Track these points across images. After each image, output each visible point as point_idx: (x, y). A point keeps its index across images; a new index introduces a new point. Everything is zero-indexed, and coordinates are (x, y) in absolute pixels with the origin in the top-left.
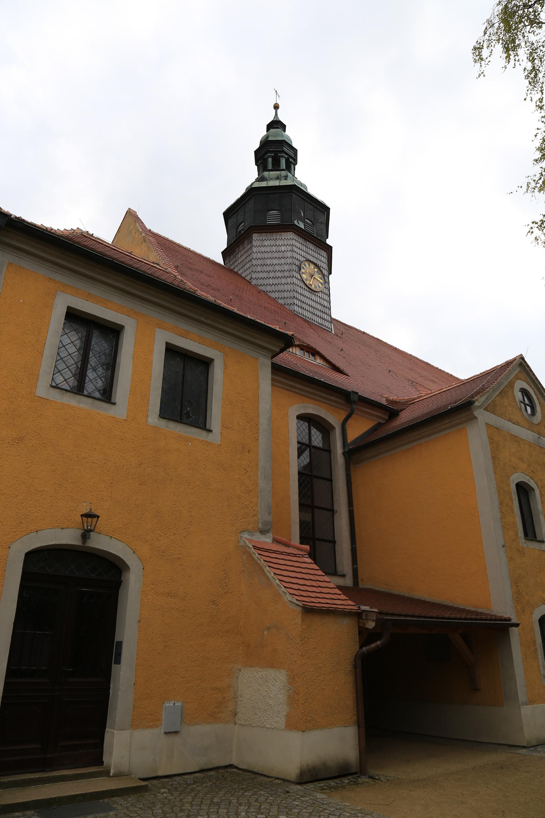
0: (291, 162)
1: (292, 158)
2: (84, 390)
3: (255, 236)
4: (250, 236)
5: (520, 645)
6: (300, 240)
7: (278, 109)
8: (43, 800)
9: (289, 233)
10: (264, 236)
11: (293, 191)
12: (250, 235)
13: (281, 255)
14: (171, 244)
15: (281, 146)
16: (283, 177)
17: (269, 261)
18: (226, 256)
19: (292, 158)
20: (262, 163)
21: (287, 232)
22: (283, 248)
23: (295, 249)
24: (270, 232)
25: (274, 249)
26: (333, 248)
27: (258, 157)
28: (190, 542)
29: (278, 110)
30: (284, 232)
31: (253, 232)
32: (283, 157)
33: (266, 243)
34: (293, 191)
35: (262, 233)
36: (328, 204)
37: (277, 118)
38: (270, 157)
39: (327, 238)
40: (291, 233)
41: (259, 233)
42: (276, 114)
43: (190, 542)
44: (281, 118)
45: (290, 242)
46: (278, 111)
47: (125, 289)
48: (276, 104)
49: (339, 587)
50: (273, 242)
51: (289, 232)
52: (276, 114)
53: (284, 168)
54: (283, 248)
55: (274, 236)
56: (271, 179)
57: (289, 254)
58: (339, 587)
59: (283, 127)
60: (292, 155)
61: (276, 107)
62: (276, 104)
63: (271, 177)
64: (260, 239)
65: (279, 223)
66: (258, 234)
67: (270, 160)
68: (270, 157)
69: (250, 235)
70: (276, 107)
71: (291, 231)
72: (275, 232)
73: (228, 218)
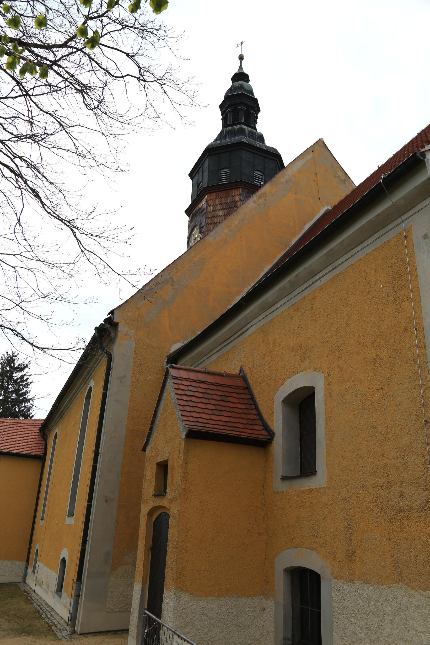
29: (243, 61)
42: (241, 67)
46: (243, 61)
61: (241, 58)
70: (241, 58)
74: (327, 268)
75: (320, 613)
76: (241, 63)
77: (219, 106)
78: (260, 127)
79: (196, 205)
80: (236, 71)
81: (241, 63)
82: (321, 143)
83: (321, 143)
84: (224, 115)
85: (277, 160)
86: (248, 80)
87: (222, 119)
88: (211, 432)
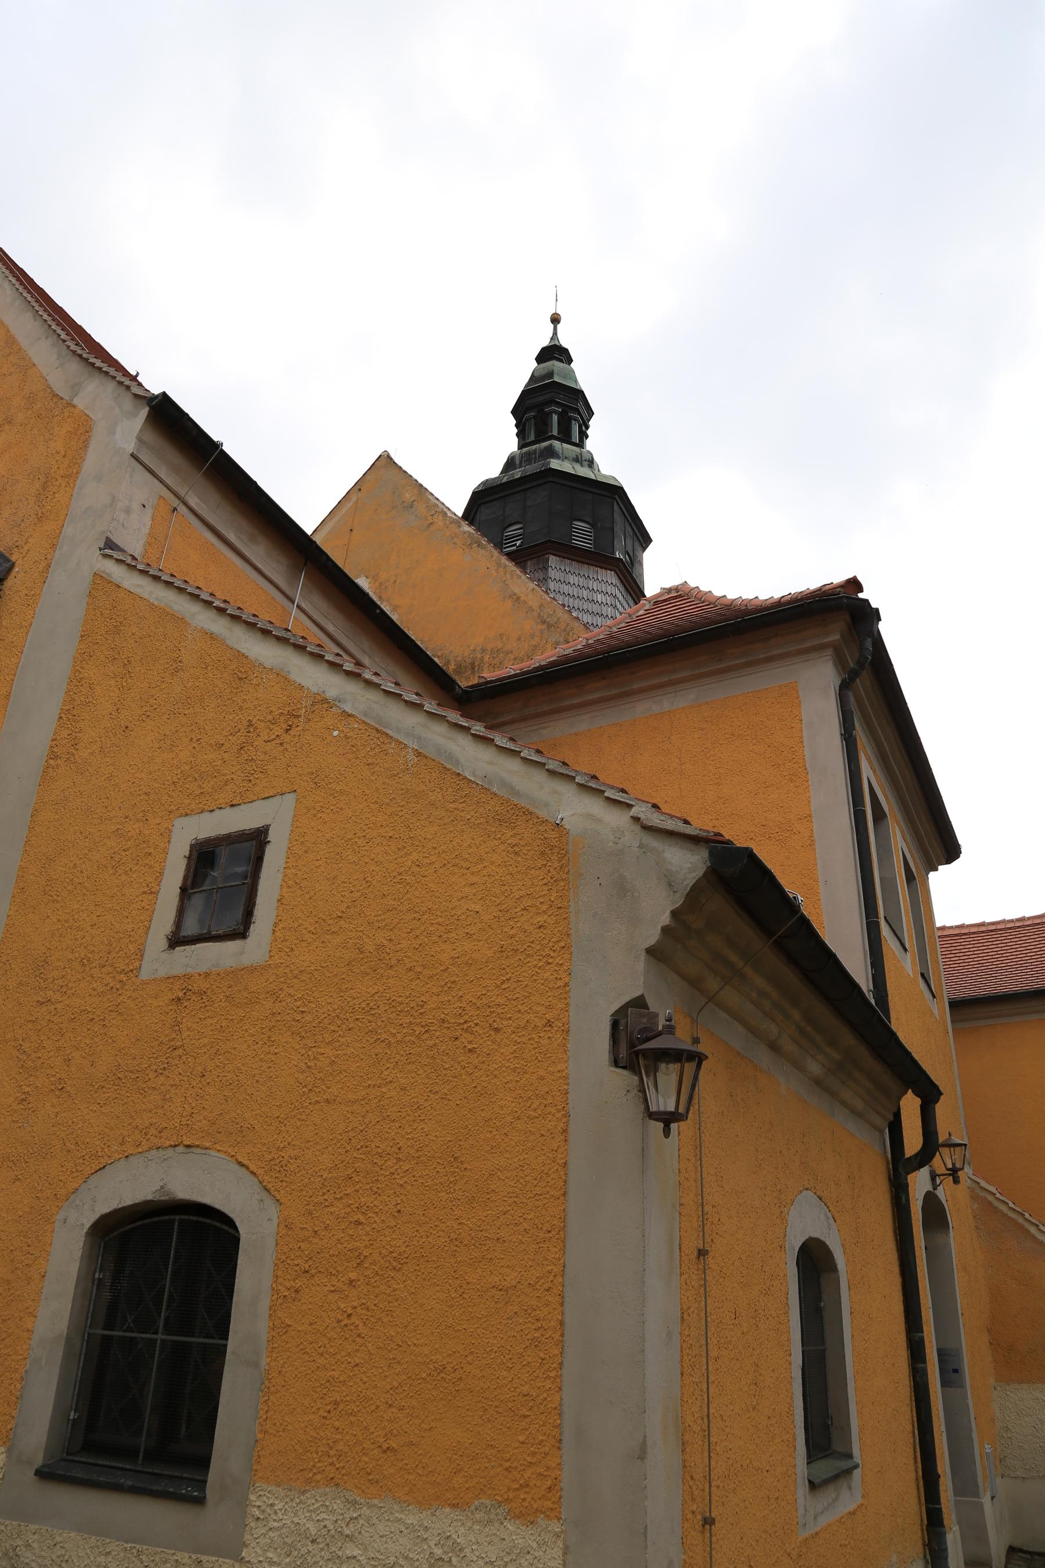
2: (934, 1155)
3: (553, 561)
4: (542, 557)
6: (622, 589)
7: (559, 323)
8: (229, 1324)
9: (609, 571)
10: (568, 565)
11: (617, 497)
12: (542, 553)
13: (595, 608)
14: (189, 423)
15: (574, 399)
16: (585, 460)
21: (606, 569)
22: (600, 597)
23: (619, 606)
24: (578, 561)
25: (585, 594)
26: (169, 393)
29: (558, 326)
30: (601, 568)
31: (550, 551)
32: (576, 420)
33: (572, 579)
34: (617, 497)
35: (564, 558)
38: (556, 412)
40: (613, 572)
41: (559, 556)
42: (555, 333)
44: (564, 343)
45: (610, 589)
46: (559, 326)
48: (556, 314)
50: (582, 581)
51: (610, 570)
52: (555, 333)
53: (555, 432)
54: (600, 597)
55: (585, 570)
56: (566, 458)
57: (609, 611)
61: (555, 320)
62: (556, 314)
63: (566, 454)
64: (560, 569)
65: (591, 548)
66: (558, 558)
67: (555, 417)
68: (556, 412)
69: (542, 553)
70: (555, 320)
71: (613, 571)
72: (587, 564)
74: (892, 933)
75: (802, 1346)
76: (555, 329)
77: (511, 412)
78: (592, 445)
79: (520, 558)
80: (546, 343)
81: (555, 329)
82: (385, 461)
83: (385, 461)
84: (521, 428)
85: (617, 569)
86: (569, 360)
87: (518, 435)
88: (614, 692)
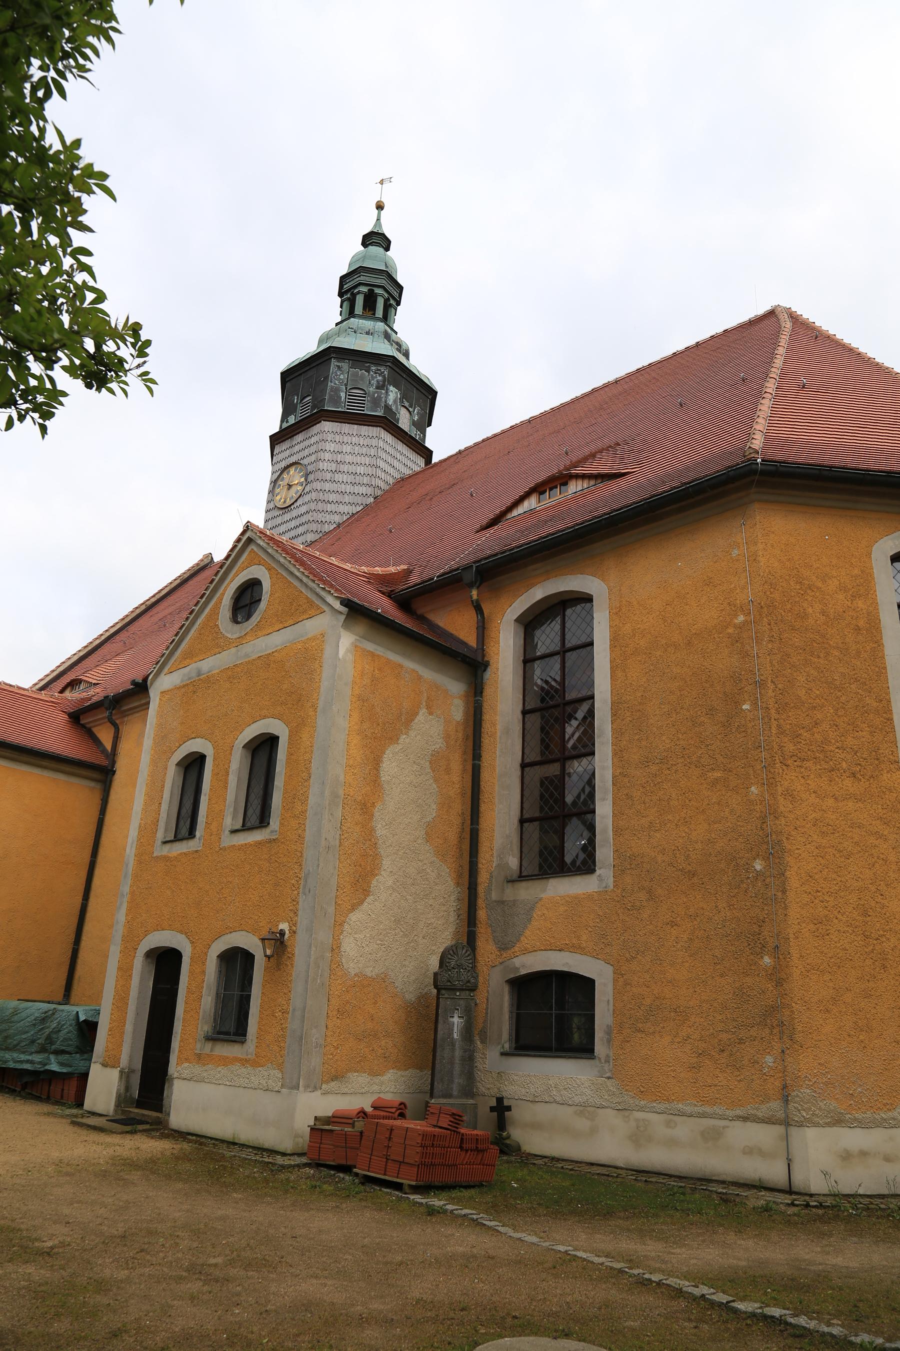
0: (391, 305)
1: (394, 298)
5: (476, 978)
7: (382, 210)
17: (345, 476)
18: (275, 443)
19: (394, 298)
20: (348, 299)
27: (345, 286)
28: (816, 1041)
36: (436, 384)
37: (380, 226)
39: (430, 424)
42: (378, 219)
43: (816, 1041)
47: (511, 1012)
49: (107, 1120)
52: (378, 219)
58: (107, 1120)
59: (386, 244)
60: (396, 294)
61: (380, 207)
73: (287, 380)
